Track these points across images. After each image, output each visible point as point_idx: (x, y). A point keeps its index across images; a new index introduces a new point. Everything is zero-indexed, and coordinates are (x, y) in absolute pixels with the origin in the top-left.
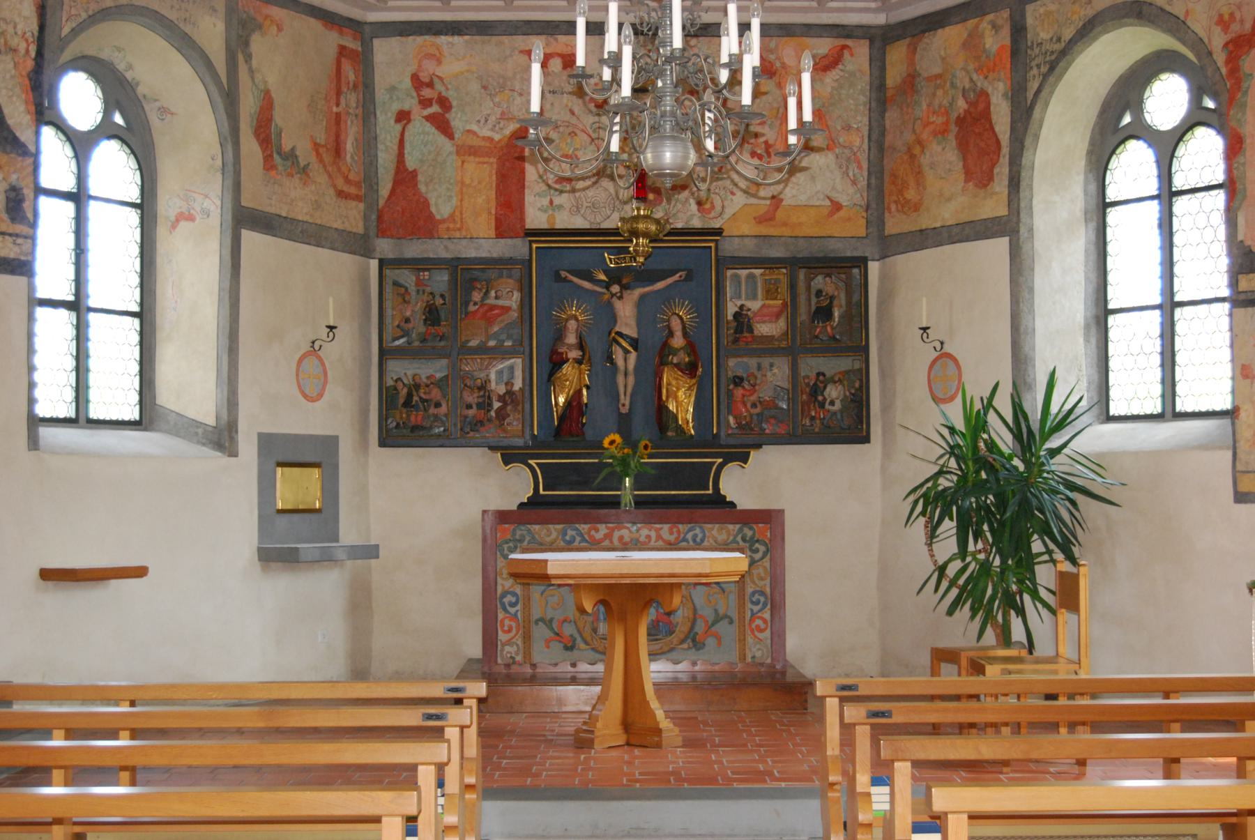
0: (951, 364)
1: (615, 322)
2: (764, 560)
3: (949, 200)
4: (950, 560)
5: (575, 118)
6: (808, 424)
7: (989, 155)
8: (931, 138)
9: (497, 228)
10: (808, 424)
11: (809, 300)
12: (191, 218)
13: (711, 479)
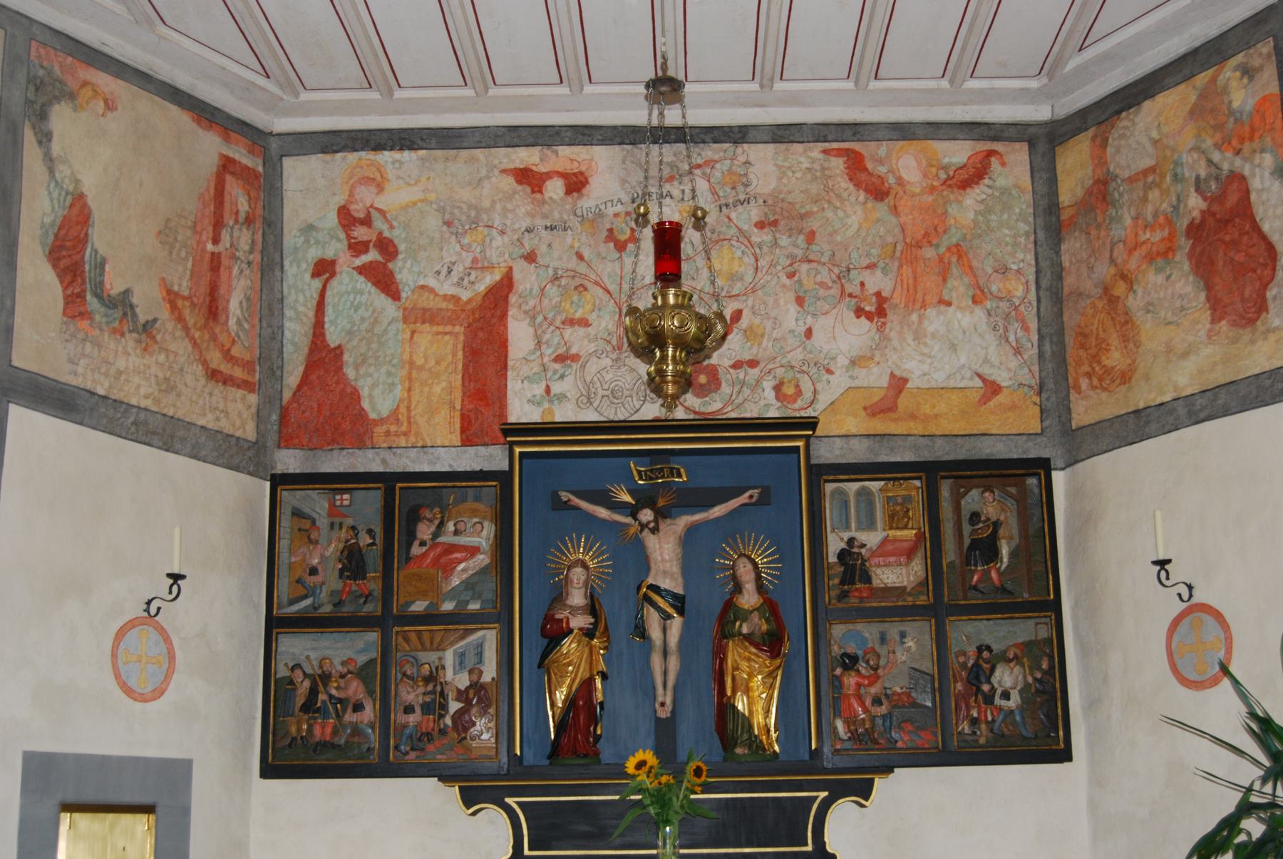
0: (1209, 620)
3: (1185, 355)
5: (583, 264)
6: (967, 730)
7: (1254, 271)
8: (1144, 267)
9: (463, 430)
10: (967, 730)
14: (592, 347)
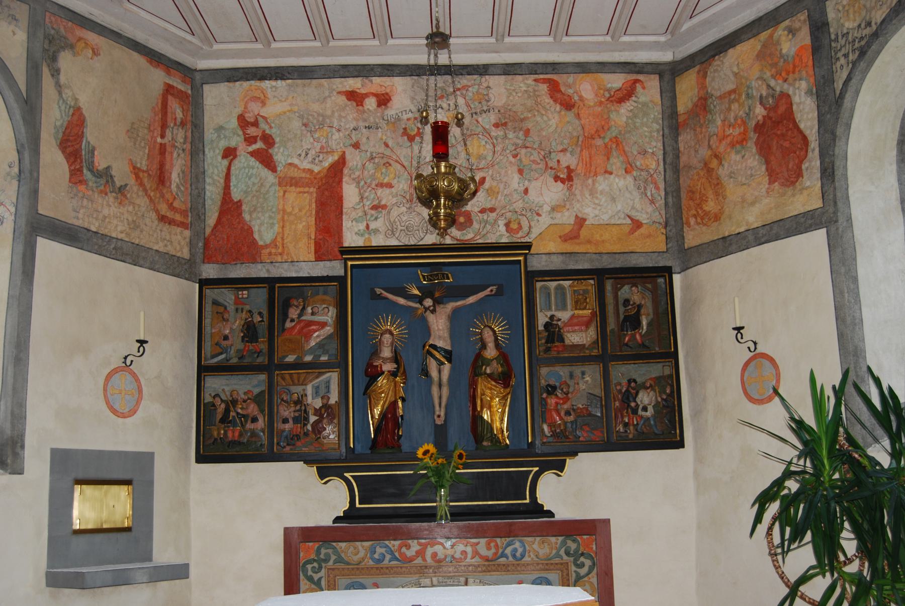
0: (766, 363)
1: (430, 335)
2: (590, 576)
3: (753, 204)
6: (622, 430)
9: (316, 252)
10: (622, 430)
13: (528, 488)
14: (394, 200)
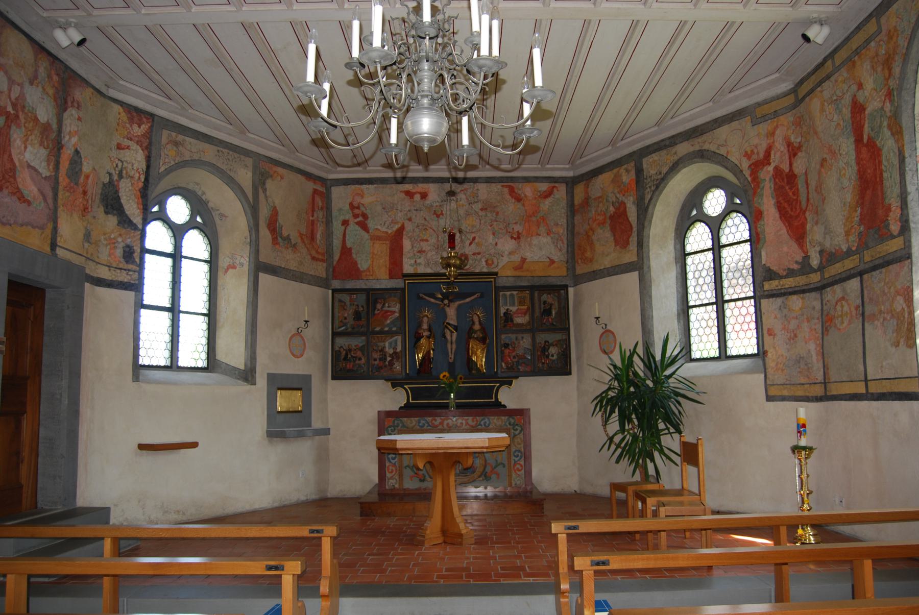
0: (611, 335)
3: (607, 256)
4: (615, 434)
9: (390, 274)
11: (540, 305)
12: (234, 267)
14: (429, 248)
